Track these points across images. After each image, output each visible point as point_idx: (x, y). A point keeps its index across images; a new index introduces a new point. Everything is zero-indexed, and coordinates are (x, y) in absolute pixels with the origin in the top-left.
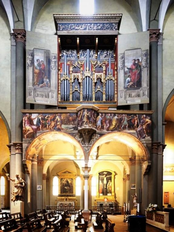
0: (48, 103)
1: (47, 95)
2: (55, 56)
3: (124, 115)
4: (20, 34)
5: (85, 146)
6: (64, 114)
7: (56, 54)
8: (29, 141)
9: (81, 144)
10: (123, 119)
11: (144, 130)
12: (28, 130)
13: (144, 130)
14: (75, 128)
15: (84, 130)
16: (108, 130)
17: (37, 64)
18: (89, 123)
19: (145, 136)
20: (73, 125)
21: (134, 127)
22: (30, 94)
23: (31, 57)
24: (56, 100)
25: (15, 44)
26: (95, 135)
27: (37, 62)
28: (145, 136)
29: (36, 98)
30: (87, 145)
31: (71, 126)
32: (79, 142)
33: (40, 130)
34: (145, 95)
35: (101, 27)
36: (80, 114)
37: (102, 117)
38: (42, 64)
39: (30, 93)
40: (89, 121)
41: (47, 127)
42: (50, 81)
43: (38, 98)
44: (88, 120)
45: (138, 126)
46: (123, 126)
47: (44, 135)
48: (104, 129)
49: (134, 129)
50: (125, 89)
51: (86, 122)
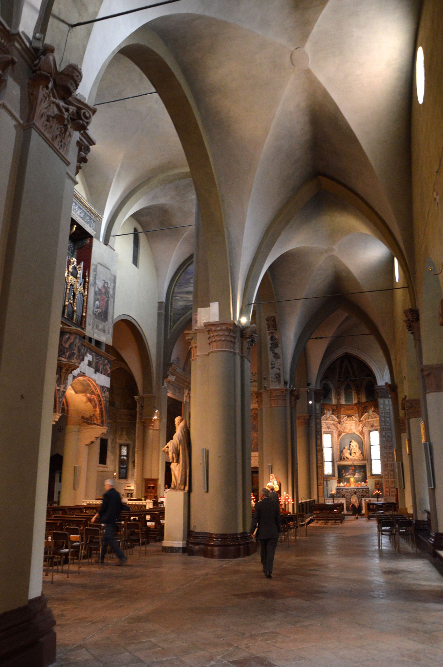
36: (69, 338)
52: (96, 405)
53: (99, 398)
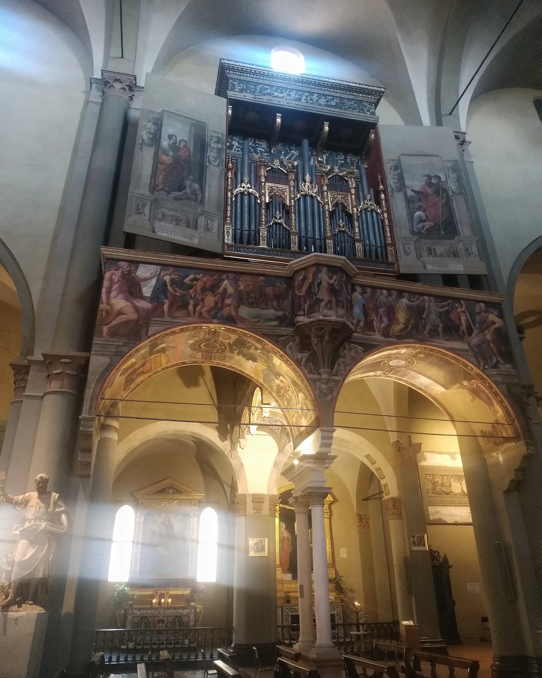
0: (195, 242)
1: (191, 222)
2: (218, 138)
3: (426, 298)
4: (121, 82)
5: (319, 380)
6: (248, 278)
7: (222, 134)
8: (118, 346)
9: (306, 371)
10: (427, 307)
11: (491, 345)
12: (120, 313)
13: (491, 345)
14: (282, 321)
15: (320, 325)
16: (386, 333)
17: (169, 145)
18: (337, 306)
19: (498, 362)
20: (276, 310)
21: (461, 333)
22: (141, 211)
23: (153, 126)
24: (218, 238)
25: (100, 101)
26: (347, 347)
27: (168, 139)
28: (498, 362)
29: (158, 225)
30: (324, 376)
31: (271, 312)
32: (298, 362)
33: (162, 314)
34: (473, 253)
35: (336, 103)
36: (305, 278)
37: (364, 297)
38: (181, 146)
39: (140, 207)
40: (338, 302)
41: (188, 309)
42: (202, 189)
43: (162, 223)
44: (333, 298)
45: (470, 331)
46: (428, 327)
47: (173, 333)
48: (374, 331)
49: (461, 338)
50: (414, 235)
51: (326, 300)
52: (489, 399)
53: (485, 383)
